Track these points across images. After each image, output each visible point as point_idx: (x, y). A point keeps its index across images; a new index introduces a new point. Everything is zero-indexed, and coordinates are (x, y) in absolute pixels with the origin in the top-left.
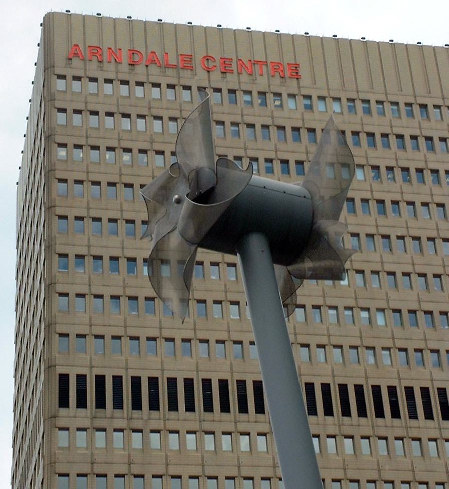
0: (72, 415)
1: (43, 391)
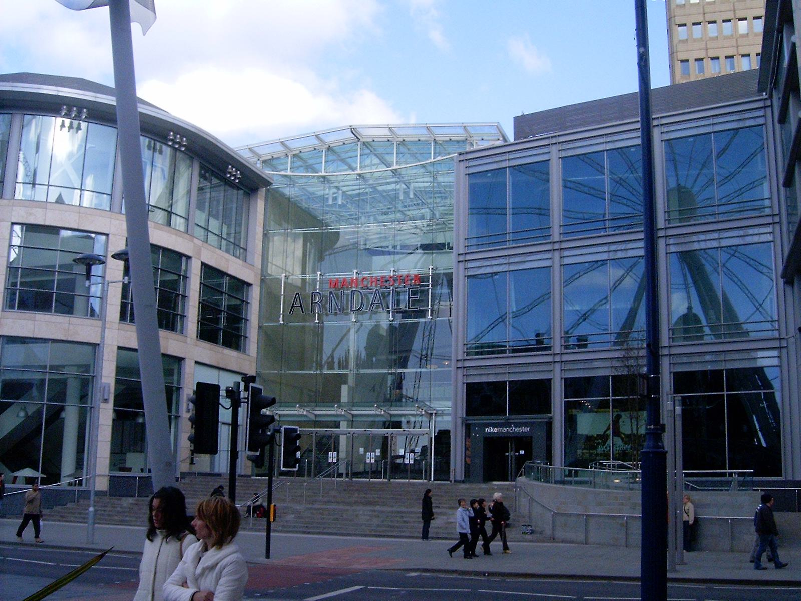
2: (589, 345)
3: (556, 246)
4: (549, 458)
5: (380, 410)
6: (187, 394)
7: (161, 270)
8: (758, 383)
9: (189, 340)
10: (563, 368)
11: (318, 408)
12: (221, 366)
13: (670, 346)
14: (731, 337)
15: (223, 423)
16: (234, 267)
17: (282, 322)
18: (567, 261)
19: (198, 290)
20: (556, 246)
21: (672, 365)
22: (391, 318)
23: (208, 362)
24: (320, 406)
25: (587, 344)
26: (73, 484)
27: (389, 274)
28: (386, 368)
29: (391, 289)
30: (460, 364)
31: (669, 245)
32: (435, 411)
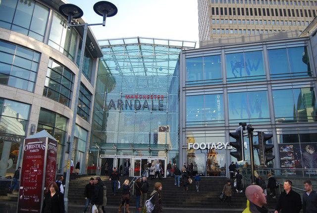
0: (215, 16)
1: (208, 12)
3: (225, 86)
16: (92, 90)
20: (225, 86)
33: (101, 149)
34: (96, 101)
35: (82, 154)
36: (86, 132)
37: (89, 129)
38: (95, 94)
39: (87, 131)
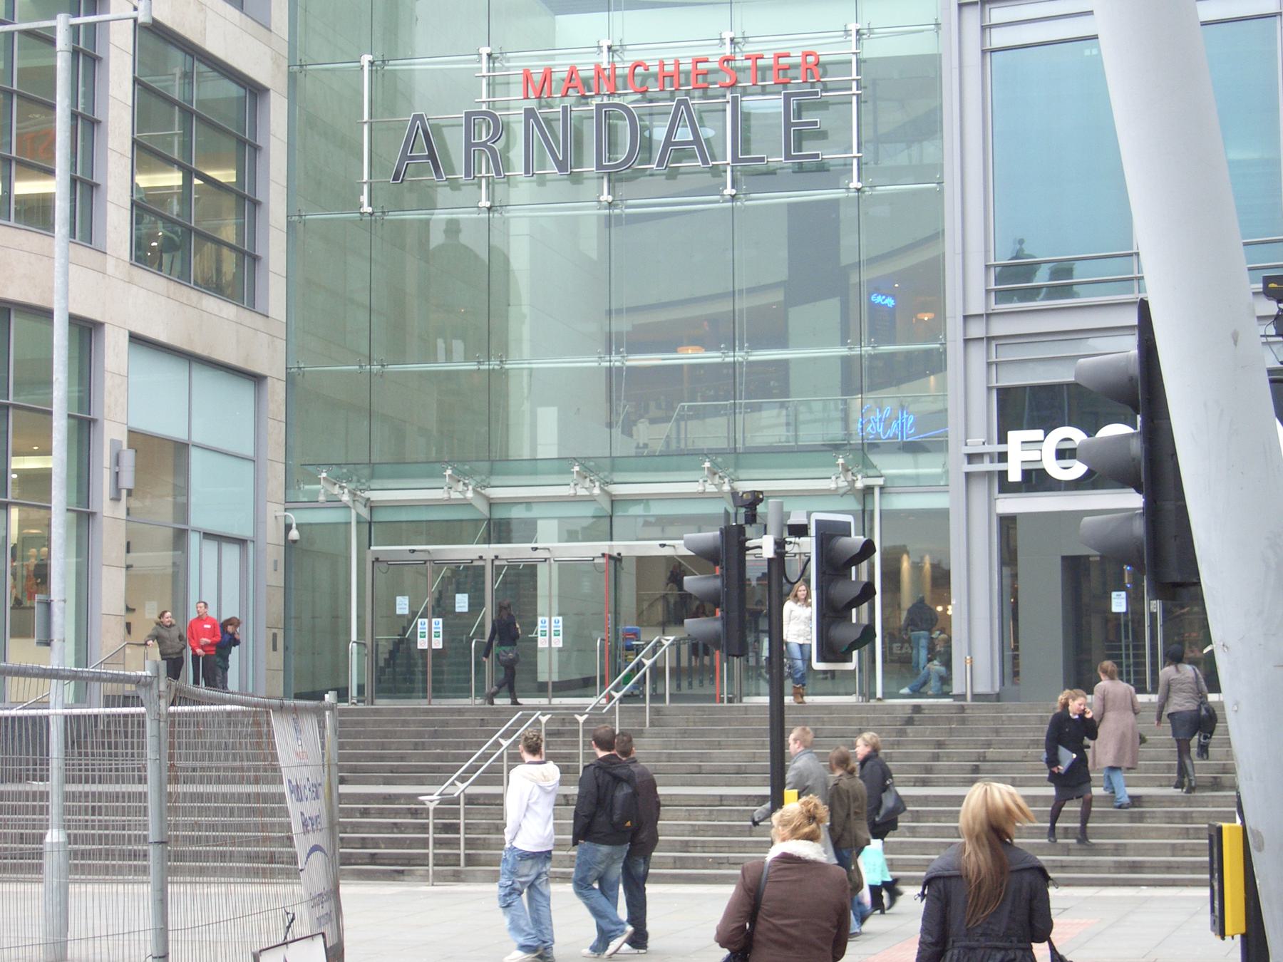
2: (1075, 288)
4: (195, 657)
5: (461, 486)
6: (112, 441)
7: (20, 96)
8: (1142, 421)
9: (111, 263)
10: (993, 359)
11: (376, 484)
12: (199, 350)
13: (988, 315)
14: (1021, 300)
15: (208, 536)
17: (370, 210)
18: (999, 38)
19: (130, 103)
21: (994, 367)
22: (606, 197)
23: (163, 338)
24: (381, 477)
25: (1071, 285)
26: (946, 688)
27: (721, 51)
28: (719, 349)
29: (729, 97)
30: (977, 330)
31: (991, 27)
32: (880, 481)
33: (372, 507)
34: (304, 123)
35: (231, 554)
36: (245, 391)
37: (269, 358)
38: (293, 79)
39: (257, 379)
